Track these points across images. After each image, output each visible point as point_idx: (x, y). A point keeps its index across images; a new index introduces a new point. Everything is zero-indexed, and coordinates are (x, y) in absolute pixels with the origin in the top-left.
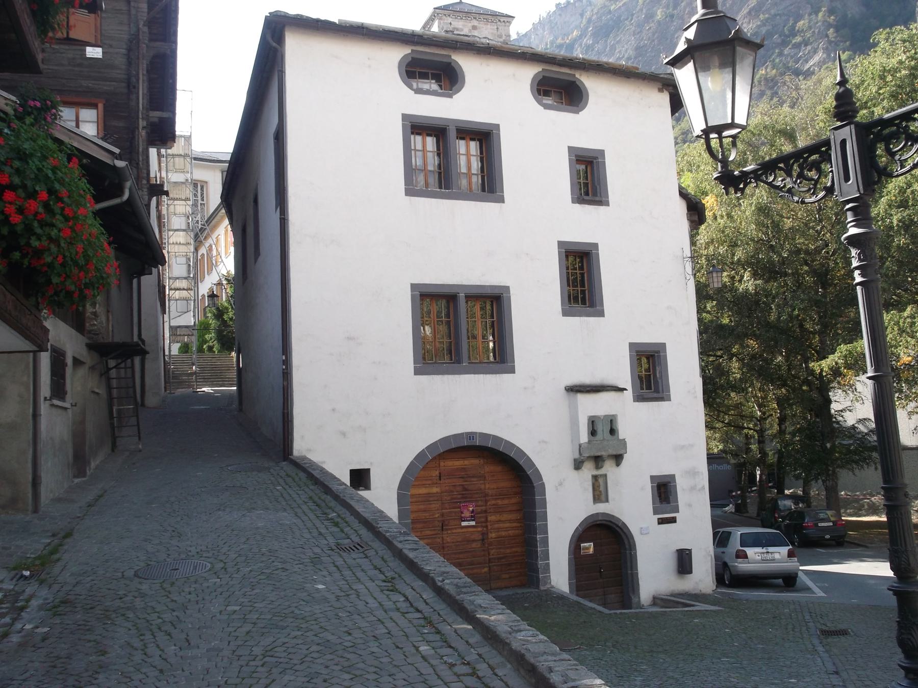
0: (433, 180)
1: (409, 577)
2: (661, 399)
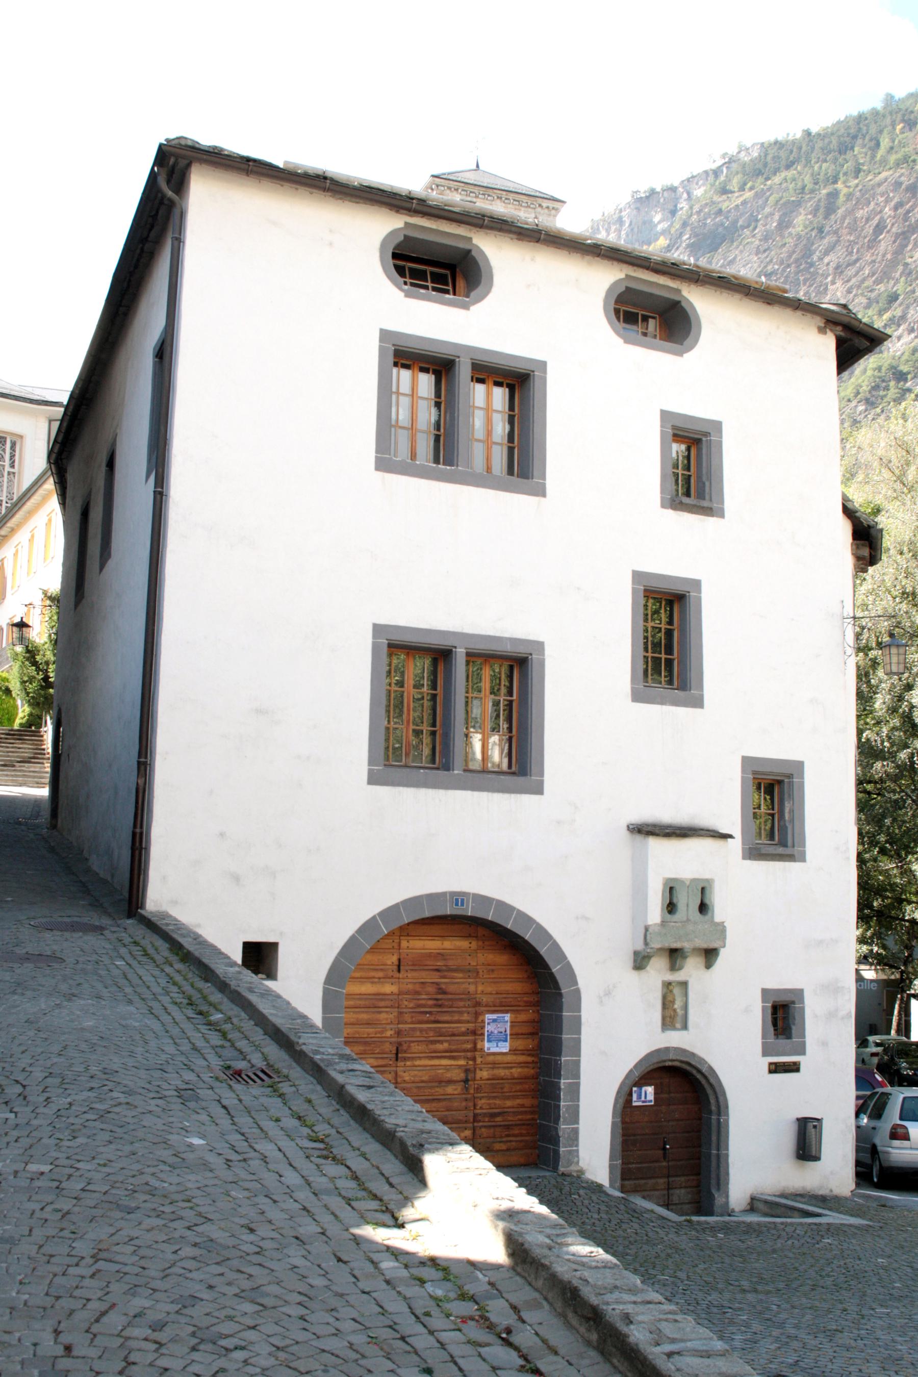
0: (425, 446)
1: (358, 1137)
2: (791, 858)
